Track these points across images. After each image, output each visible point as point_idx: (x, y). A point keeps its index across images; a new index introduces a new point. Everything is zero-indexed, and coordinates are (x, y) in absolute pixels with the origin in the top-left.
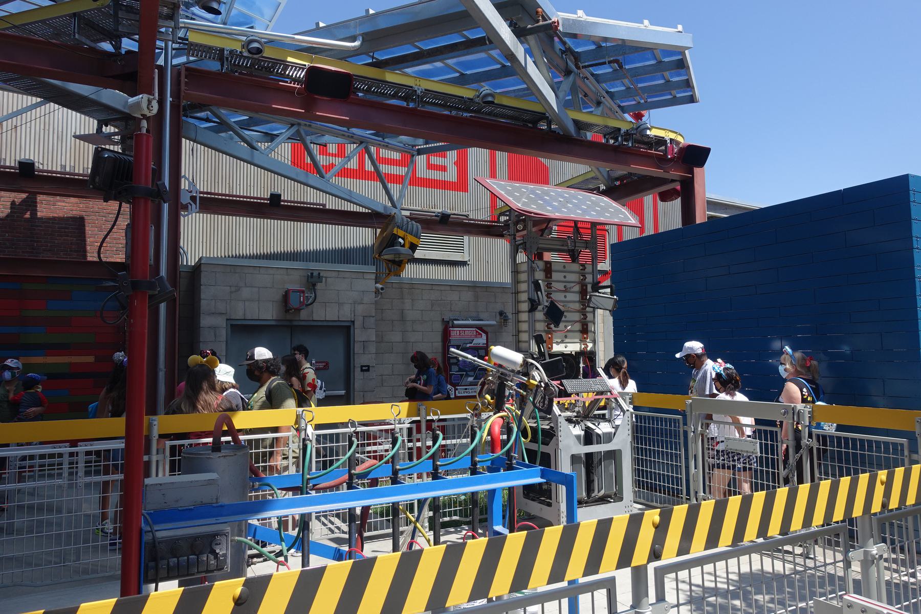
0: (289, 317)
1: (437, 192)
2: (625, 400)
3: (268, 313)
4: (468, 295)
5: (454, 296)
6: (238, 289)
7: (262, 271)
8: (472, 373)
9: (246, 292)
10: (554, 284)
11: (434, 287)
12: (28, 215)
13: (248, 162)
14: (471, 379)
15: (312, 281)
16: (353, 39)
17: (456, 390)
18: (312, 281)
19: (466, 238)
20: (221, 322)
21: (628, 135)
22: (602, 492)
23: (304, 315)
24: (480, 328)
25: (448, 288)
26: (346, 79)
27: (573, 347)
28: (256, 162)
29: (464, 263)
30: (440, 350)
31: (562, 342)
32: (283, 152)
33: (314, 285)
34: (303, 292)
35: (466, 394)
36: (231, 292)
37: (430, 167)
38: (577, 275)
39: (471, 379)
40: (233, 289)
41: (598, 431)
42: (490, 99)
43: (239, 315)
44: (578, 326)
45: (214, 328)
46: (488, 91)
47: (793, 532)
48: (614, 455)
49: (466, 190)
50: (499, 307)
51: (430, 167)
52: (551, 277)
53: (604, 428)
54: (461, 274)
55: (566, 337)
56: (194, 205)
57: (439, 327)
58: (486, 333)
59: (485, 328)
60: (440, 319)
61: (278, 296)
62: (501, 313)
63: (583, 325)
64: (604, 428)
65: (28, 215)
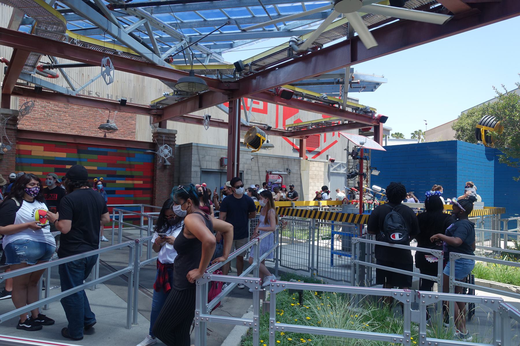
3: (215, 166)
7: (213, 149)
20: (198, 169)
24: (280, 175)
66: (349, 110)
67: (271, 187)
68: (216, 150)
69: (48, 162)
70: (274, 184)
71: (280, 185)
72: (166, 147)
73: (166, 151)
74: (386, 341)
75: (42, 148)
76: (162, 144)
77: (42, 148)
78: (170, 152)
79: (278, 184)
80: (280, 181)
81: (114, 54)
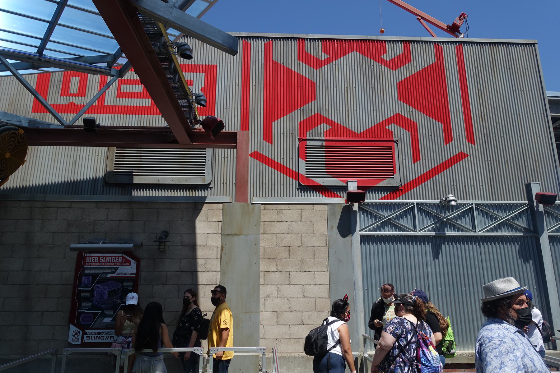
11: (74, 205)
17: (84, 333)
35: (100, 341)
58: (138, 260)
67: (92, 292)
70: (104, 281)
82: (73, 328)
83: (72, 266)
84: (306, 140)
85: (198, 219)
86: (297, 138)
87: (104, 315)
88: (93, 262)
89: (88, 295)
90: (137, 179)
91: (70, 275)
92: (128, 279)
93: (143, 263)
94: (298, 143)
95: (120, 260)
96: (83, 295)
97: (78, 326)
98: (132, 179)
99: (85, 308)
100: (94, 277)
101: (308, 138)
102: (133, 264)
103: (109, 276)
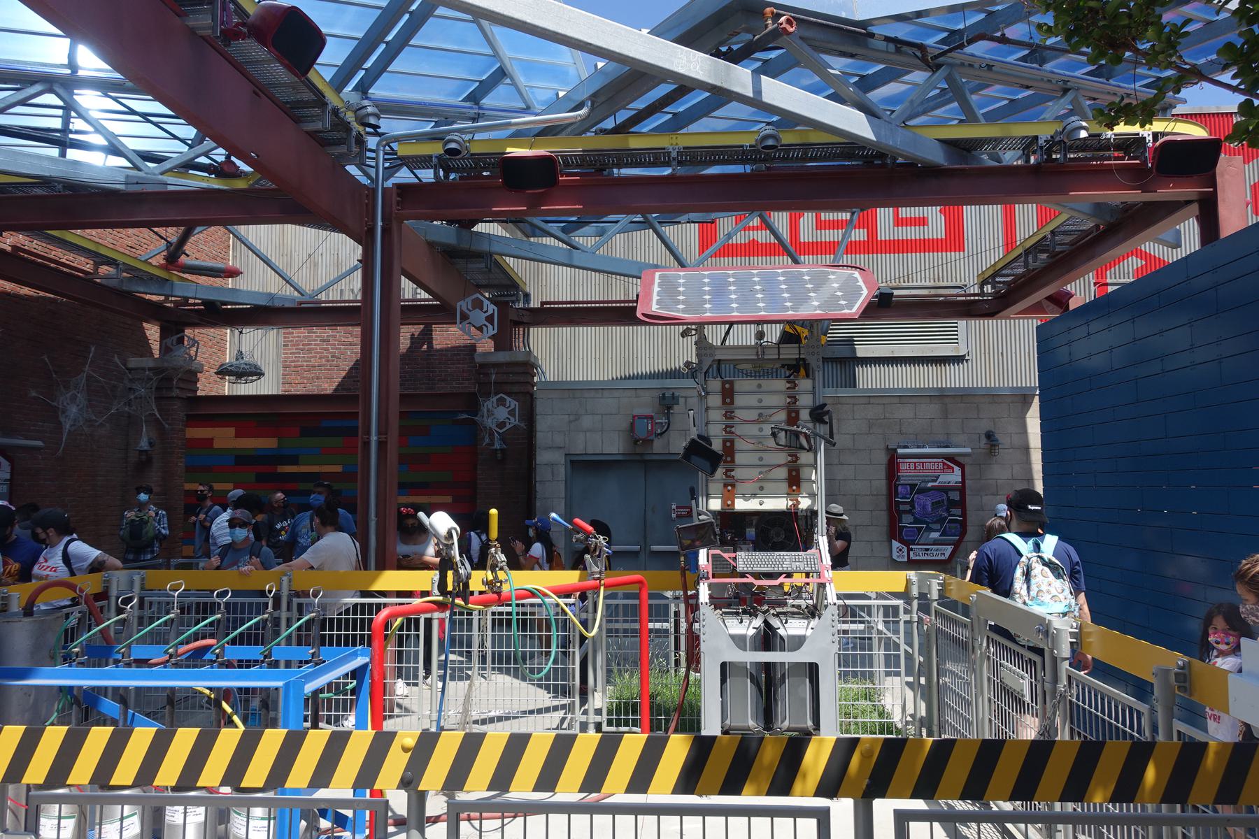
0: (638, 450)
1: (912, 257)
2: (565, 593)
3: (613, 445)
4: (932, 410)
5: (905, 412)
6: (578, 417)
7: (606, 393)
8: (937, 526)
9: (587, 421)
10: (738, 413)
11: (872, 400)
12: (425, 347)
13: (567, 265)
14: (935, 535)
15: (667, 403)
16: (579, 107)
17: (909, 550)
18: (667, 403)
19: (962, 324)
20: (558, 457)
21: (1053, 143)
22: (786, 723)
23: (658, 446)
24: (951, 458)
25: (897, 400)
26: (546, 163)
27: (777, 504)
28: (575, 263)
29: (959, 359)
30: (884, 490)
31: (754, 496)
32: (756, 221)
33: (669, 408)
34: (651, 417)
35: (926, 558)
36: (570, 422)
37: (899, 222)
38: (783, 397)
39: (935, 535)
40: (572, 418)
41: (781, 632)
42: (770, 142)
43: (579, 449)
44: (782, 473)
45: (552, 465)
46: (768, 132)
47: (157, 788)
48: (812, 671)
49: (961, 248)
50: (985, 426)
51: (899, 222)
52: (732, 403)
53: (794, 627)
54: (954, 378)
55: (761, 488)
56: (490, 327)
57: (882, 458)
58: (962, 466)
59: (960, 460)
60: (883, 446)
61: (625, 425)
62: (989, 436)
63: (790, 472)
64: (794, 627)
65: (425, 347)
66: (1011, 157)
67: (912, 503)
68: (616, 394)
69: (243, 460)
70: (923, 491)
71: (955, 496)
72: (501, 402)
73: (501, 413)
74: (323, 806)
75: (231, 431)
76: (487, 395)
77: (231, 431)
78: (512, 413)
79: (945, 490)
80: (954, 477)
81: (437, 124)
82: (895, 544)
83: (881, 473)
84: (1107, 285)
85: (1029, 415)
86: (1092, 282)
87: (930, 530)
88: (907, 470)
89: (907, 507)
90: (862, 351)
91: (881, 484)
92: (953, 489)
93: (967, 469)
94: (1093, 288)
95: (941, 466)
96: (902, 507)
97: (902, 541)
98: (854, 351)
99: (907, 520)
100: (913, 486)
101: (1109, 280)
102: (957, 470)
103: (930, 485)
